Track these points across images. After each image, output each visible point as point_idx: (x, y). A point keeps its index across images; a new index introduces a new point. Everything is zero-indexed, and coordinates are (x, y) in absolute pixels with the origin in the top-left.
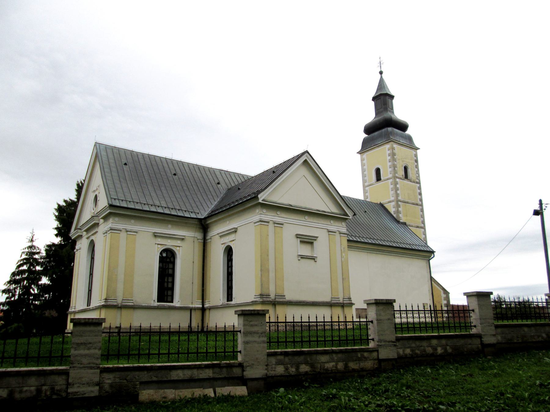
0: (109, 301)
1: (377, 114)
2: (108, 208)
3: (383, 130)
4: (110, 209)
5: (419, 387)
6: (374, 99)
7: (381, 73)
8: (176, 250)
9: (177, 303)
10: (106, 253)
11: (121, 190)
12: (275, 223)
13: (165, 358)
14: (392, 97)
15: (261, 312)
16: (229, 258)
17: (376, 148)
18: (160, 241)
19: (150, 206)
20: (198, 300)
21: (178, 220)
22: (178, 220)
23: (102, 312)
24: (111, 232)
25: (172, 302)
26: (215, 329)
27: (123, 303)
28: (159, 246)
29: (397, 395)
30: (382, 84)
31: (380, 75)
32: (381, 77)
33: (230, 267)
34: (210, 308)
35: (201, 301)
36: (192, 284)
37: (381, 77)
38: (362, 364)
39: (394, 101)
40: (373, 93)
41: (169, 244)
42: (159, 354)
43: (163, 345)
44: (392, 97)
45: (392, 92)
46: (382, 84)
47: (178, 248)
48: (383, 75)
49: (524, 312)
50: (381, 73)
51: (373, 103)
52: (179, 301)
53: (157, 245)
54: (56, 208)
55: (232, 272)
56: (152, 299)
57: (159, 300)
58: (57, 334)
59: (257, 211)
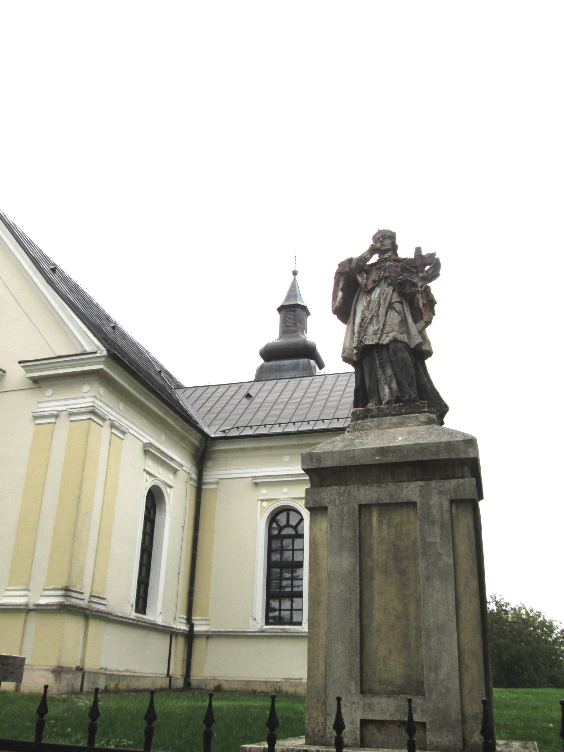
0: (74, 594)
1: (280, 337)
2: (103, 359)
3: (301, 361)
4: (105, 363)
6: (280, 309)
7: (295, 273)
12: (71, 414)
21: (177, 427)
22: (177, 427)
23: (28, 628)
24: (90, 419)
26: (31, 725)
27: (93, 605)
28: (265, 504)
30: (293, 291)
31: (293, 276)
32: (295, 279)
34: (208, 636)
35: (185, 617)
36: (177, 575)
37: (295, 279)
46: (293, 291)
48: (297, 277)
49: (371, 698)
50: (295, 273)
52: (161, 613)
53: (145, 473)
54: (424, 253)
56: (129, 601)
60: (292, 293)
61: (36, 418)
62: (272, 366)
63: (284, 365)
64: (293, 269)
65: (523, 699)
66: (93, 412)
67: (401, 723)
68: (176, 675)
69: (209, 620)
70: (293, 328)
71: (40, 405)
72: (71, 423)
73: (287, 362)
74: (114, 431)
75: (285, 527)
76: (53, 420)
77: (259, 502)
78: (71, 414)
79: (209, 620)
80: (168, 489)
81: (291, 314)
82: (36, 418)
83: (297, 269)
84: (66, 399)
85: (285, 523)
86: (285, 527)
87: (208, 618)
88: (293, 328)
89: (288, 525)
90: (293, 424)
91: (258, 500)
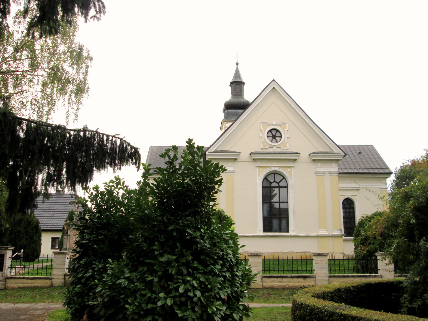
6: (232, 83)
7: (237, 64)
8: (354, 198)
9: (292, 232)
11: (353, 155)
12: (330, 173)
13: (300, 272)
14: (244, 83)
19: (379, 169)
25: (288, 231)
28: (341, 197)
30: (237, 74)
32: (237, 68)
37: (237, 68)
38: (8, 235)
40: (231, 79)
41: (348, 195)
42: (279, 270)
43: (337, 266)
44: (244, 83)
45: (244, 79)
46: (237, 74)
47: (355, 197)
48: (238, 66)
50: (237, 64)
57: (264, 231)
58: (27, 262)
60: (238, 75)
61: (316, 173)
62: (233, 112)
64: (236, 62)
65: (249, 256)
67: (42, 269)
70: (240, 94)
71: (317, 169)
72: (119, 134)
75: (273, 182)
76: (323, 175)
78: (330, 173)
80: (289, 170)
81: (238, 86)
82: (316, 173)
83: (238, 62)
86: (273, 182)
88: (240, 94)
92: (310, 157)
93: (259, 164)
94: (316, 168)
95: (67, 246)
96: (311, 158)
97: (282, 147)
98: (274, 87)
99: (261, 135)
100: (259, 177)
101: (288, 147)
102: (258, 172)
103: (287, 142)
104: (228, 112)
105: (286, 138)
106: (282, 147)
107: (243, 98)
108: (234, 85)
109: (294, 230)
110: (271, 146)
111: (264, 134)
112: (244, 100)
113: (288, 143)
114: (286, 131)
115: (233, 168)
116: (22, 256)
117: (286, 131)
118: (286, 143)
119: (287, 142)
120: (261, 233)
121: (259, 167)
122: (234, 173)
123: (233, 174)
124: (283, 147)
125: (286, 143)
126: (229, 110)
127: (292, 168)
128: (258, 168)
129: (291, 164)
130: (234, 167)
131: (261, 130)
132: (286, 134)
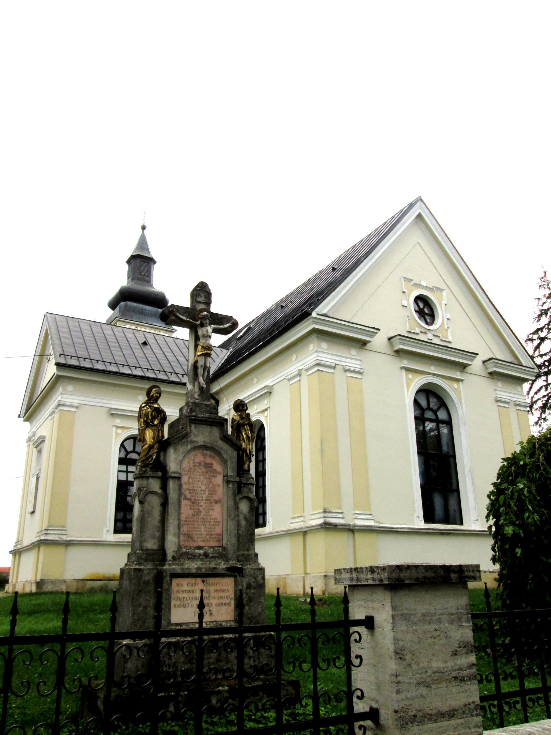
5: (468, 671)
6: (128, 262)
7: (144, 228)
10: (52, 445)
14: (155, 262)
15: (238, 593)
16: (259, 446)
17: (147, 328)
18: (118, 422)
20: (313, 510)
25: (462, 524)
28: (119, 431)
29: (504, 666)
30: (143, 243)
31: (142, 231)
32: (143, 233)
33: (261, 461)
37: (143, 233)
39: (155, 265)
40: (130, 251)
44: (155, 262)
45: (154, 254)
46: (143, 243)
48: (145, 231)
50: (144, 228)
51: (127, 265)
55: (265, 470)
59: (311, 347)
61: (497, 401)
63: (146, 310)
64: (142, 224)
66: (318, 365)
68: (36, 580)
69: (65, 530)
73: (148, 308)
74: (349, 374)
75: (131, 452)
77: (114, 428)
79: (65, 530)
80: (455, 385)
83: (146, 225)
84: (511, 393)
85: (131, 449)
86: (131, 452)
87: (65, 529)
89: (134, 451)
90: (70, 357)
91: (113, 426)
92: (485, 366)
93: (406, 363)
94: (496, 390)
95: (162, 540)
96: (486, 368)
97: (441, 338)
98: (419, 216)
99: (405, 303)
100: (408, 392)
101: (450, 339)
102: (404, 380)
103: (448, 328)
104: (126, 306)
105: (445, 320)
106: (441, 338)
107: (152, 286)
108: (138, 261)
109: (478, 520)
110: (422, 330)
111: (408, 301)
112: (151, 289)
113: (449, 330)
114: (443, 306)
115: (359, 363)
116: (206, 652)
117: (443, 306)
118: (446, 330)
119: (448, 328)
120: (421, 524)
121: (408, 370)
122: (361, 373)
123: (359, 376)
124: (443, 336)
125: (446, 330)
126: (129, 303)
127: (461, 383)
128: (404, 372)
129: (457, 375)
130: (360, 360)
131: (404, 292)
132: (444, 312)
